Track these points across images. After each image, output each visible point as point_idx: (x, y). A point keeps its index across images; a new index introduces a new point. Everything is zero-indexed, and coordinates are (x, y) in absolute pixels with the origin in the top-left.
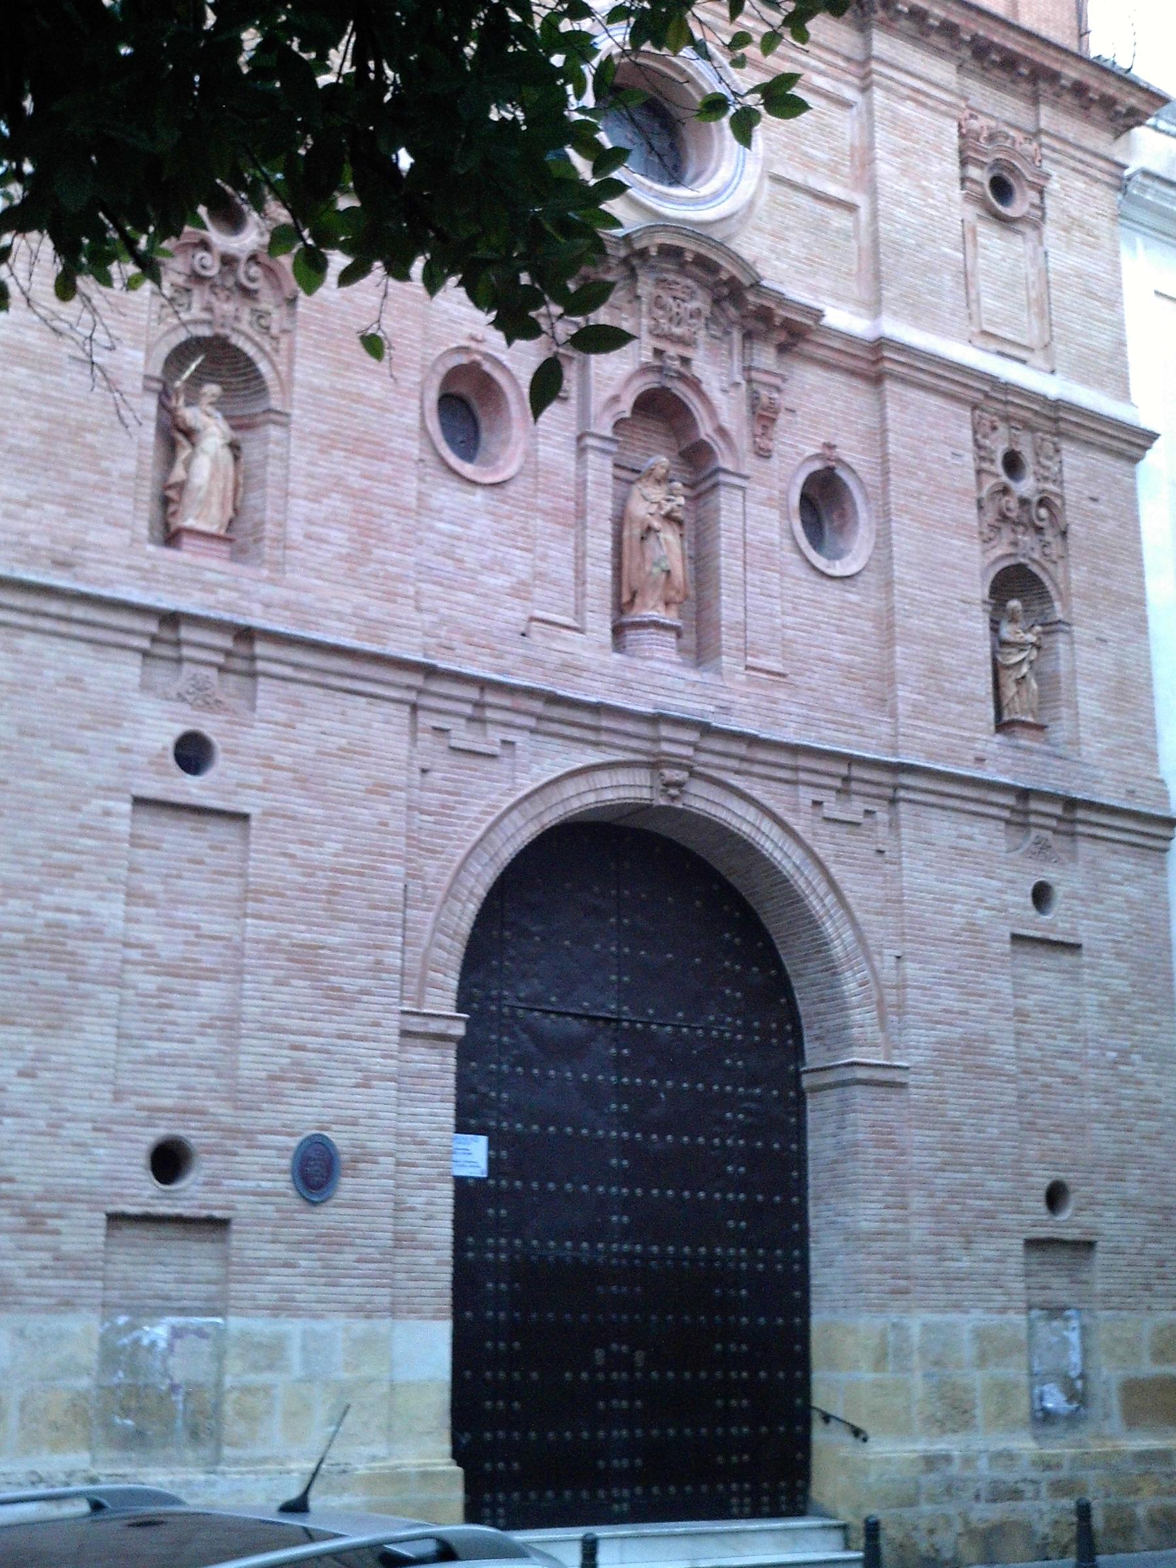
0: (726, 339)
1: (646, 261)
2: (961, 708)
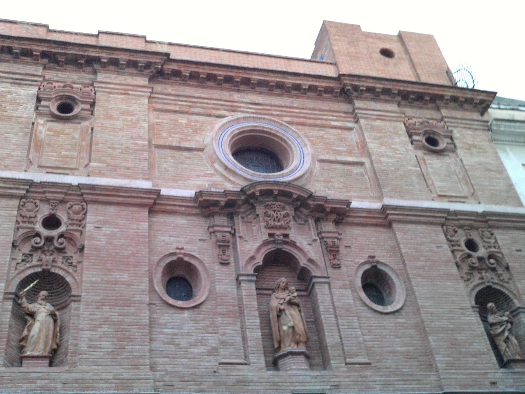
0: (306, 223)
1: (257, 199)
2: (475, 359)
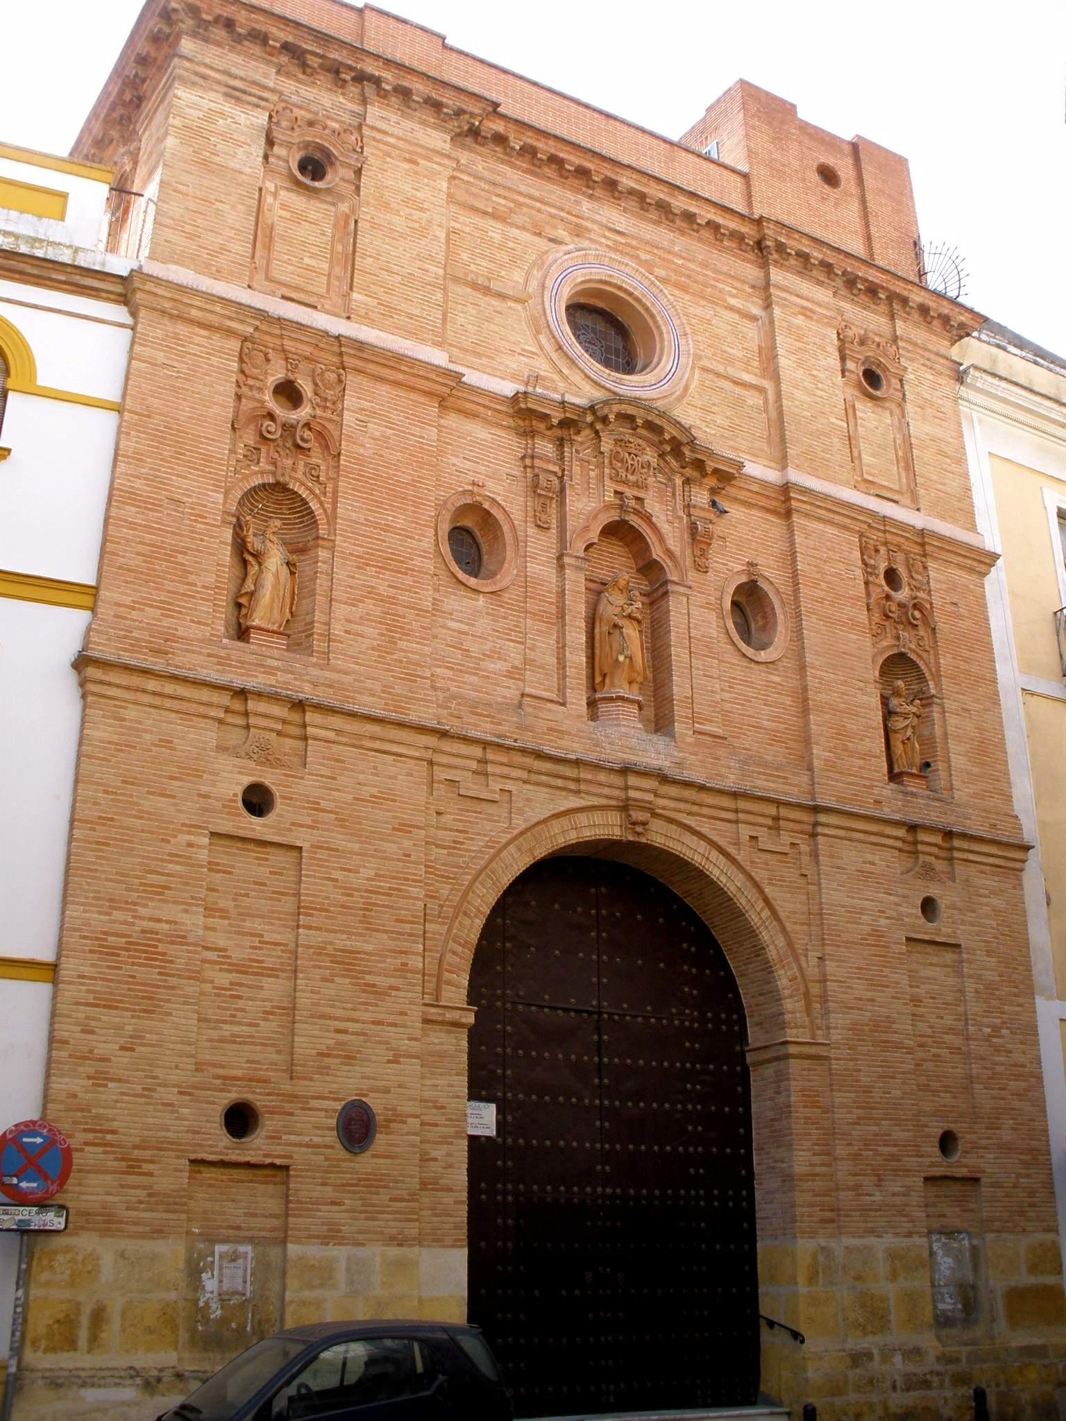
2: (861, 762)
